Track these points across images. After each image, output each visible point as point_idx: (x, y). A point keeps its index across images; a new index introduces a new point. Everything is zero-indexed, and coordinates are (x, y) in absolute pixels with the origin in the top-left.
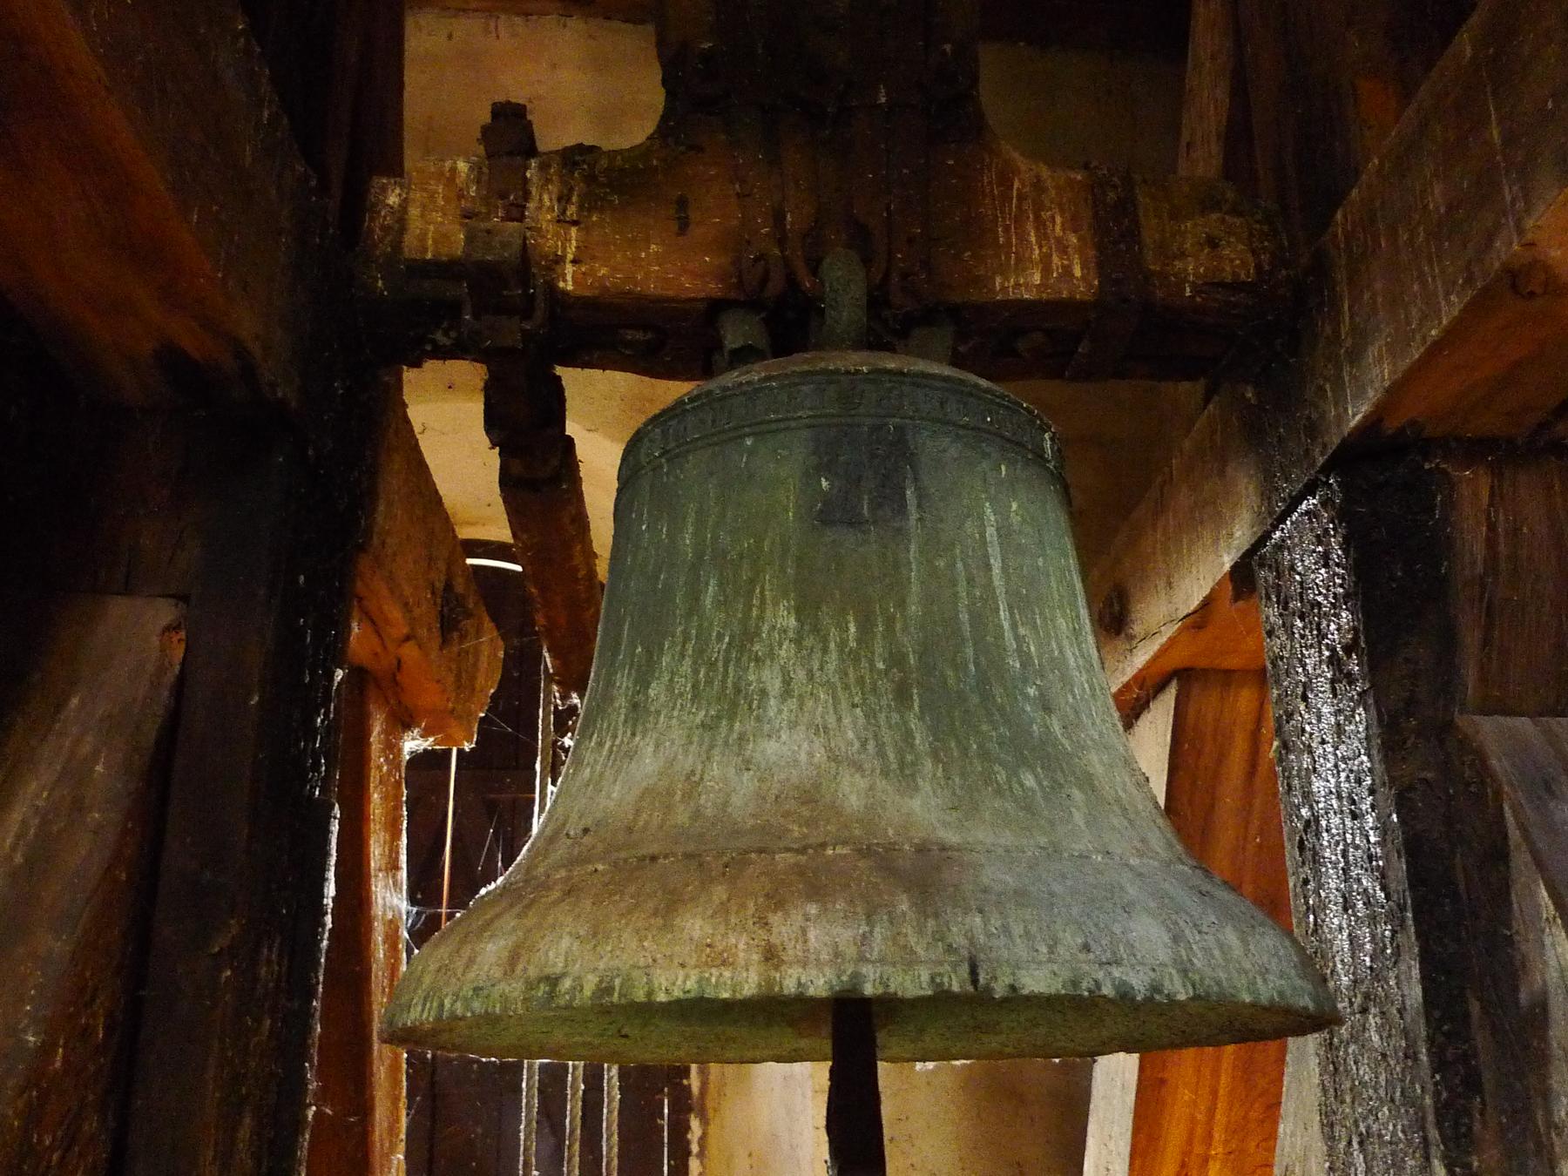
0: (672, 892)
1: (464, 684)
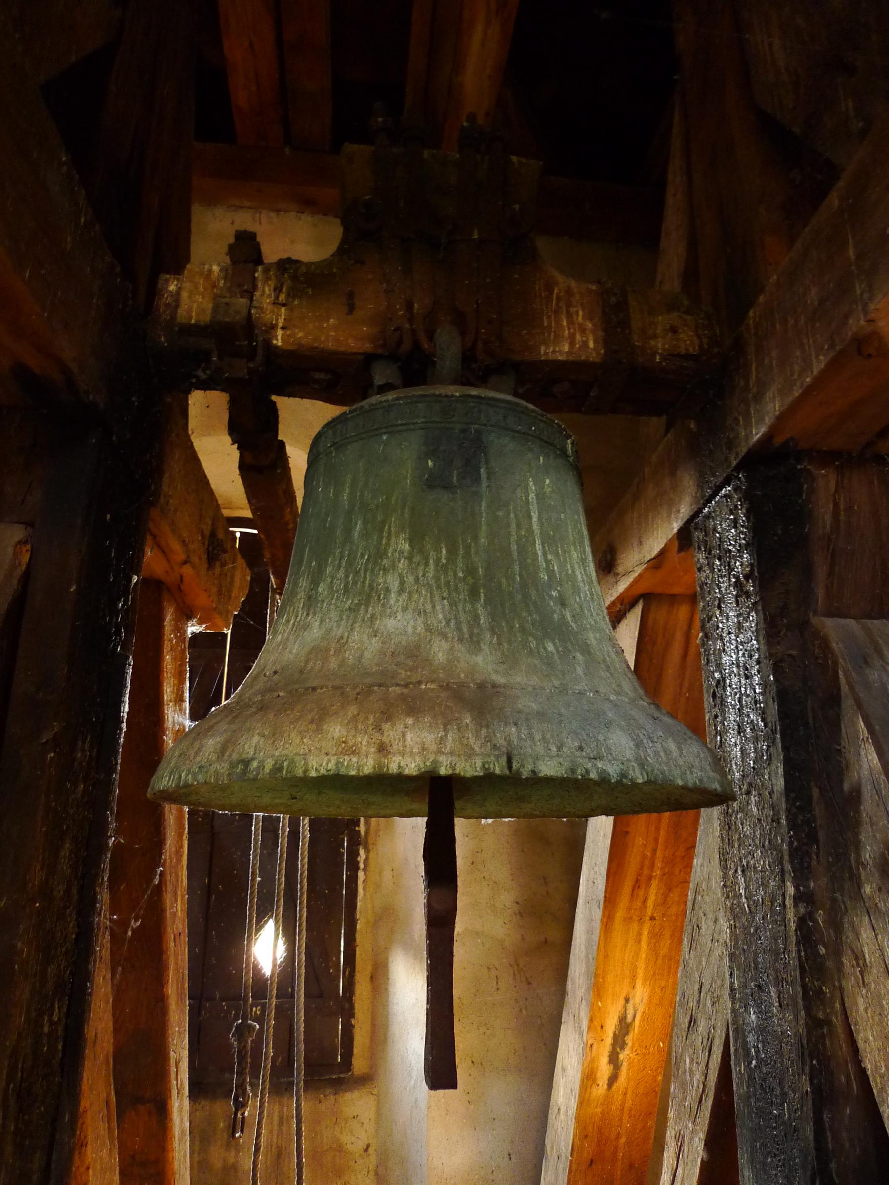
0: (322, 709)
1: (224, 593)
